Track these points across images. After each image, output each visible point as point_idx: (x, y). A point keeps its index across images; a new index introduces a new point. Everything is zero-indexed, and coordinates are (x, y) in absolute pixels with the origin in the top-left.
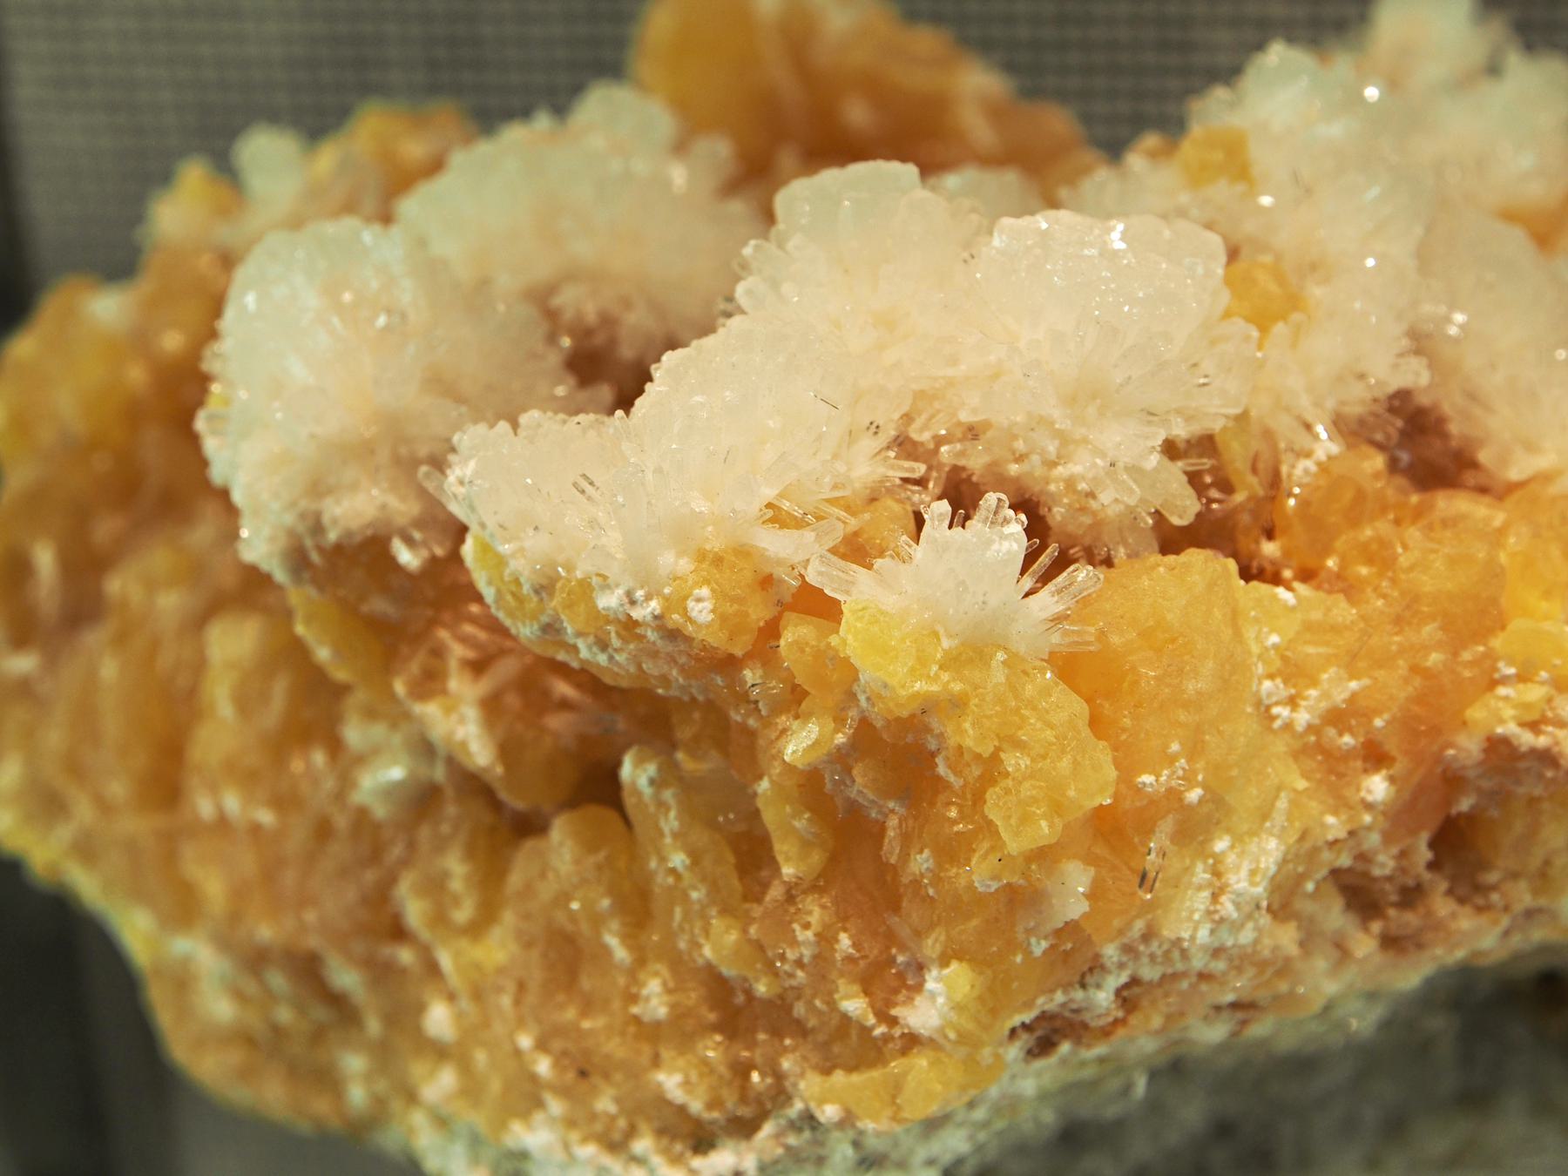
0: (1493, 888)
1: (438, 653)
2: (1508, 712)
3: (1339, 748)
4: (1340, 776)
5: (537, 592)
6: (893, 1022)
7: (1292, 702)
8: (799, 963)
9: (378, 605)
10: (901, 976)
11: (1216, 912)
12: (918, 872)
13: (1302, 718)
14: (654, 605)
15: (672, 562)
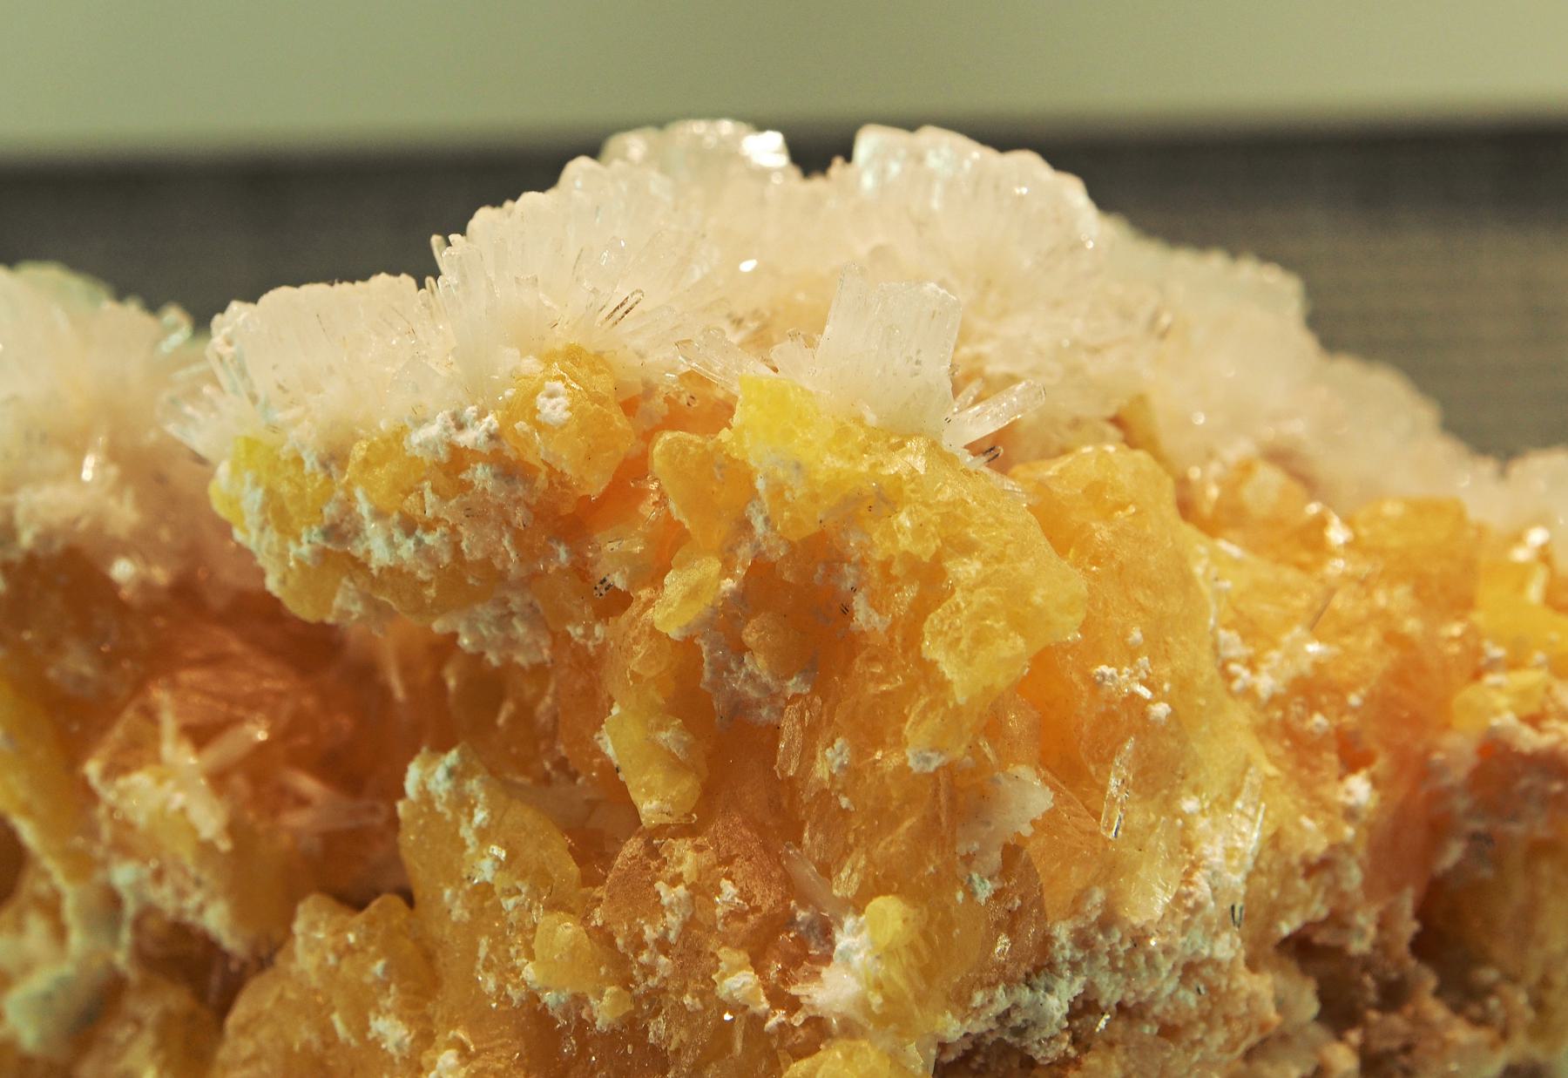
0: (1490, 990)
1: (150, 714)
2: (1502, 701)
3: (1311, 733)
4: (1314, 769)
5: (324, 465)
6: (794, 1005)
7: (1251, 664)
8: (663, 946)
9: (76, 663)
10: (801, 942)
11: (1190, 895)
12: (826, 777)
13: (1265, 684)
14: (491, 421)
15: (514, 361)
